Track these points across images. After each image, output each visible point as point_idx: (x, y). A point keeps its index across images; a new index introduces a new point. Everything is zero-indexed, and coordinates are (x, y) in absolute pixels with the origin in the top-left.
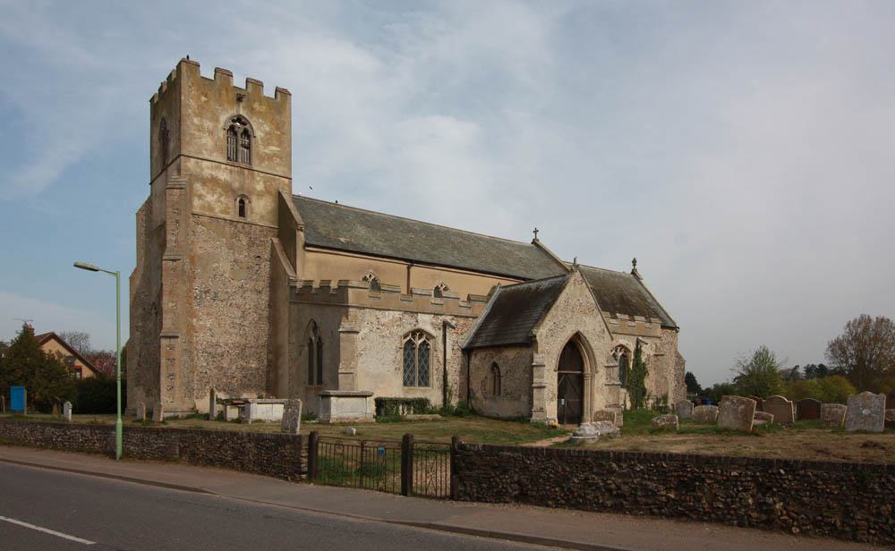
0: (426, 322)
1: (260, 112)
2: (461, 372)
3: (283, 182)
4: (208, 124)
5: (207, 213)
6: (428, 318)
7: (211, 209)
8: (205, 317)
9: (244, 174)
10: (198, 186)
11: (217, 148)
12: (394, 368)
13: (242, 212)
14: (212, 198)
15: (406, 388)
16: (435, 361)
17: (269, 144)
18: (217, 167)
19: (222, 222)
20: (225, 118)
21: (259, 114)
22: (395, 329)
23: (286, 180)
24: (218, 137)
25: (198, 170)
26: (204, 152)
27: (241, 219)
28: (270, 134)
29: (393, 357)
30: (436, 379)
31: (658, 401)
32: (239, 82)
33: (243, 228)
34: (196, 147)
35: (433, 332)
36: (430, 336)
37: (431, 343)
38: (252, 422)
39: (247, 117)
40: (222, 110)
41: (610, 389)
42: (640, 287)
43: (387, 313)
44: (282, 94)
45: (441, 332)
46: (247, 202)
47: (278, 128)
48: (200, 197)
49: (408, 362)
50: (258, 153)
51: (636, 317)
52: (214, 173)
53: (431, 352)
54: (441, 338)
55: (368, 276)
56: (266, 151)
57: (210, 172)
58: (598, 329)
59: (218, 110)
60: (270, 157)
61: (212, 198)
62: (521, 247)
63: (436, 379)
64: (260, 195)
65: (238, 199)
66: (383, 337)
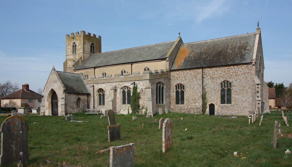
10: (68, 61)
17: (79, 46)
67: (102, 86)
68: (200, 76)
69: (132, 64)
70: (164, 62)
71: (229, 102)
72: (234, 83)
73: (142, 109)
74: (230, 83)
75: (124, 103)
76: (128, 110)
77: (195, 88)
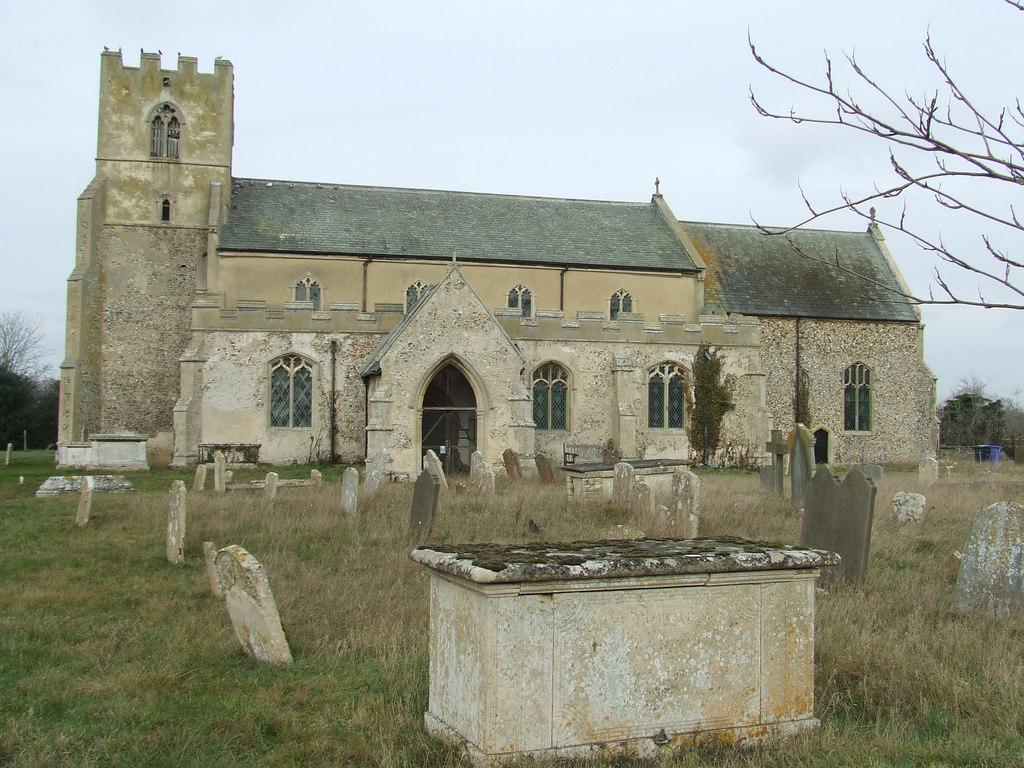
0: (304, 344)
1: (191, 94)
3: (218, 172)
4: (129, 119)
6: (308, 338)
7: (128, 215)
8: (116, 342)
10: (114, 192)
11: (138, 145)
13: (166, 215)
17: (202, 130)
18: (137, 167)
19: (140, 230)
23: (222, 170)
24: (141, 132)
26: (123, 152)
28: (203, 118)
29: (253, 391)
33: (165, 233)
35: (314, 356)
37: (313, 372)
39: (175, 102)
42: (874, 253)
43: (245, 334)
45: (329, 356)
48: (116, 204)
50: (188, 142)
52: (133, 175)
53: (314, 380)
55: (304, 281)
57: (128, 173)
58: (492, 348)
60: (202, 145)
64: (187, 192)
65: (161, 201)
67: (562, 353)
68: (789, 342)
70: (689, 282)
71: (864, 425)
72: (879, 372)
74: (868, 372)
75: (655, 420)
77: (776, 380)
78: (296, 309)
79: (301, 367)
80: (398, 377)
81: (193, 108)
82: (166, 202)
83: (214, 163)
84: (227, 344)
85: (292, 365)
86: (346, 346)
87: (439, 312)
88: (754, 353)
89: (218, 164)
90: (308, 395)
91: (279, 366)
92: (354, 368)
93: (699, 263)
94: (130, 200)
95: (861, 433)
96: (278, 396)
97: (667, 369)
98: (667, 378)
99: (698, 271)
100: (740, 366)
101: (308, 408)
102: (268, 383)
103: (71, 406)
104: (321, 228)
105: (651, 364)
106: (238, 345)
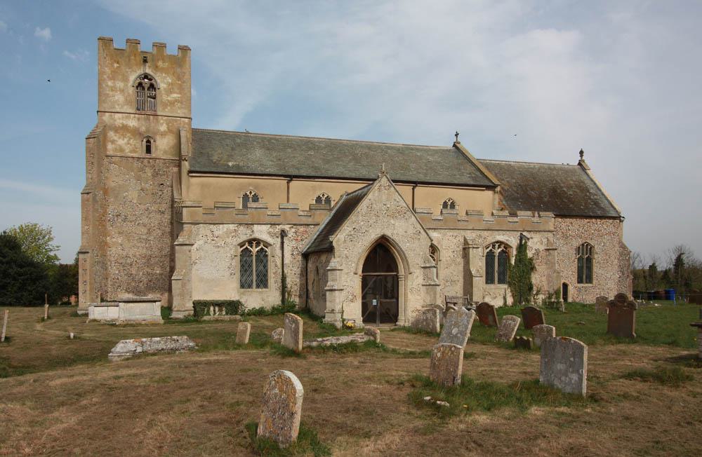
0: (262, 232)
2: (301, 274)
4: (120, 84)
5: (119, 154)
7: (122, 150)
9: (149, 120)
10: (111, 134)
11: (128, 102)
12: (228, 273)
13: (148, 150)
14: (123, 142)
15: (243, 290)
16: (273, 264)
17: (171, 93)
18: (127, 117)
19: (130, 160)
20: (133, 77)
21: (162, 70)
22: (229, 240)
23: (186, 120)
24: (129, 93)
25: (112, 121)
26: (117, 107)
27: (148, 156)
30: (274, 281)
31: (550, 297)
32: (172, 50)
33: (149, 162)
34: (110, 103)
35: (270, 240)
36: (267, 245)
38: (90, 322)
40: (131, 72)
41: (427, 289)
42: (585, 177)
43: (221, 226)
44: (184, 49)
45: (279, 240)
46: (152, 141)
47: (179, 79)
48: (113, 142)
49: (246, 267)
50: (162, 101)
51: (519, 213)
52: (124, 122)
53: (269, 257)
54: (279, 245)
55: (248, 193)
56: (169, 98)
57: (121, 121)
58: (411, 231)
59: (127, 72)
60: (172, 103)
61: (123, 142)
62: (444, 152)
63: (274, 281)
64: (163, 134)
65: (145, 140)
66: (219, 247)
69: (291, 180)
70: (490, 193)
72: (597, 249)
73: (537, 294)
74: (591, 248)
75: (490, 280)
76: (505, 299)
78: (256, 208)
79: (260, 247)
80: (346, 252)
81: (165, 78)
82: (148, 142)
83: (181, 115)
84: (209, 233)
85: (254, 245)
86: (291, 233)
87: (374, 206)
88: (550, 235)
89: (183, 116)
90: (265, 266)
91: (245, 247)
92: (297, 248)
93: (496, 181)
94: (123, 140)
95: (586, 285)
96: (245, 267)
97: (497, 245)
98: (497, 251)
99: (495, 186)
100: (542, 244)
101: (265, 275)
102: (238, 258)
103: (88, 278)
104: (257, 159)
105: (488, 243)
106: (216, 233)
